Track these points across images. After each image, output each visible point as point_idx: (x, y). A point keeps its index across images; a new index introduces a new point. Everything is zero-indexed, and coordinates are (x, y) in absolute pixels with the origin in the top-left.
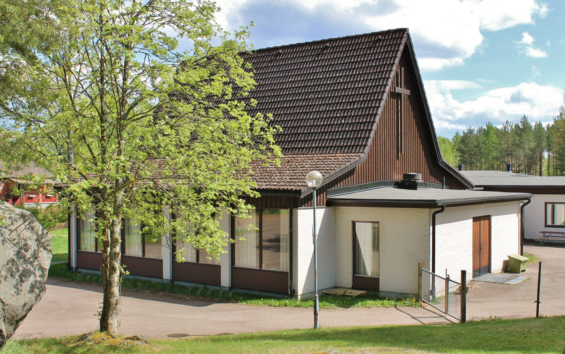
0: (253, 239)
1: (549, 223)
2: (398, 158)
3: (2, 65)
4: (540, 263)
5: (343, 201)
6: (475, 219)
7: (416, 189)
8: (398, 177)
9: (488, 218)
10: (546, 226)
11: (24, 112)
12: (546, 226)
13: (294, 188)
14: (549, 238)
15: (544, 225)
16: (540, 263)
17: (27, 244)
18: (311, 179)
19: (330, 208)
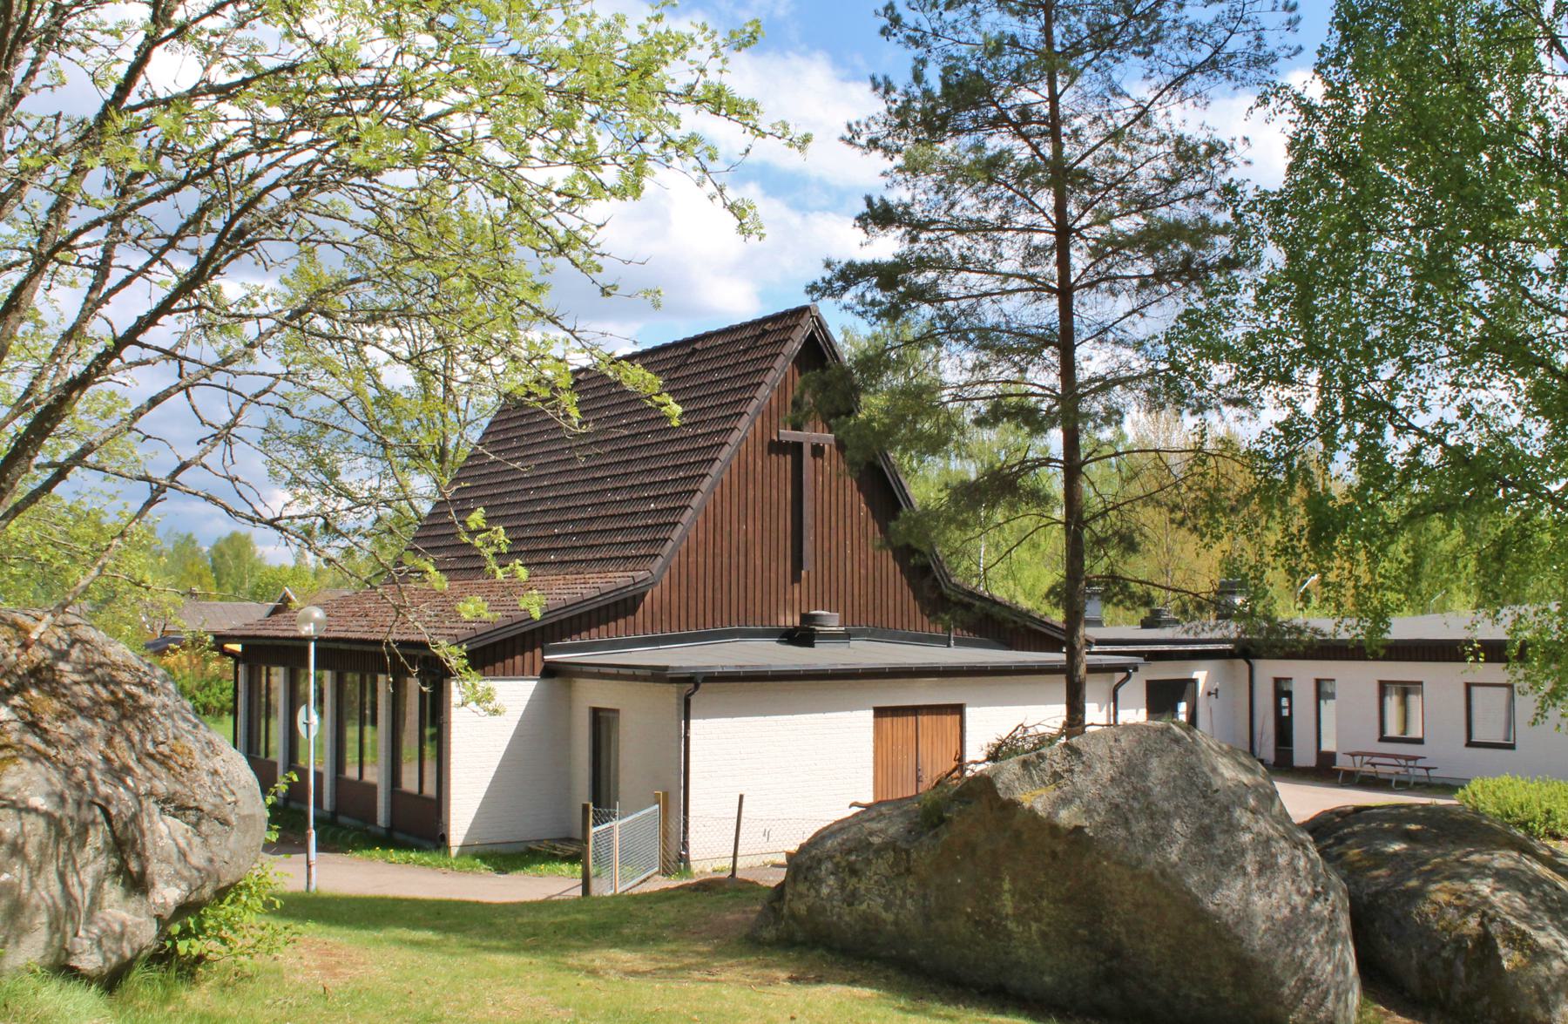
0: (1374, 765)
1: (1393, 730)
2: (796, 577)
3: (1273, 21)
4: (741, 797)
5: (595, 670)
6: (880, 712)
7: (812, 645)
8: (791, 620)
9: (958, 710)
10: (1383, 739)
11: (105, 416)
12: (1383, 739)
13: (372, 637)
14: (1379, 768)
15: (1377, 736)
16: (741, 797)
17: (1112, 779)
18: (307, 620)
19: (549, 681)
